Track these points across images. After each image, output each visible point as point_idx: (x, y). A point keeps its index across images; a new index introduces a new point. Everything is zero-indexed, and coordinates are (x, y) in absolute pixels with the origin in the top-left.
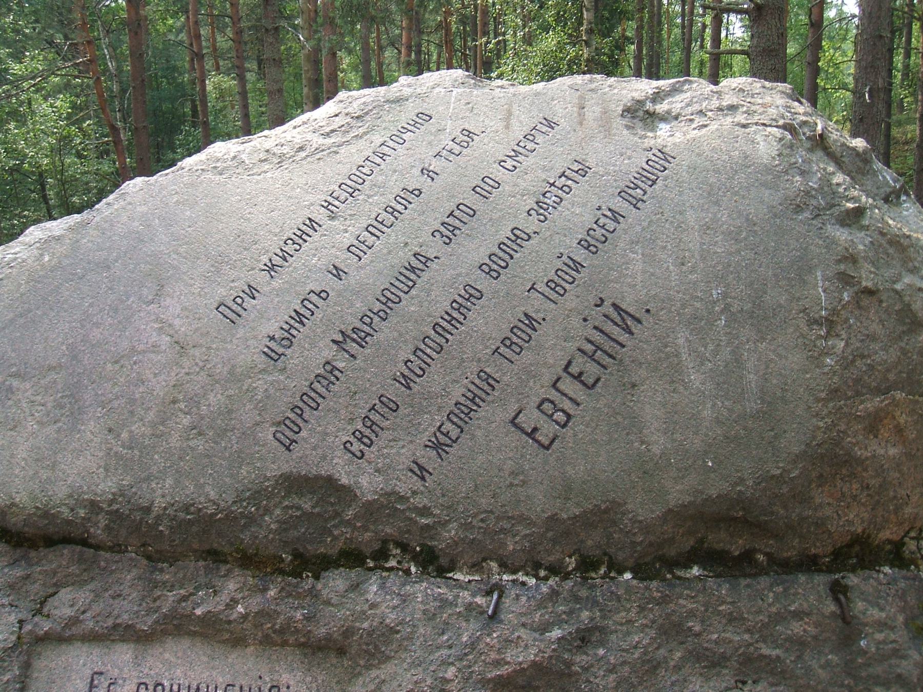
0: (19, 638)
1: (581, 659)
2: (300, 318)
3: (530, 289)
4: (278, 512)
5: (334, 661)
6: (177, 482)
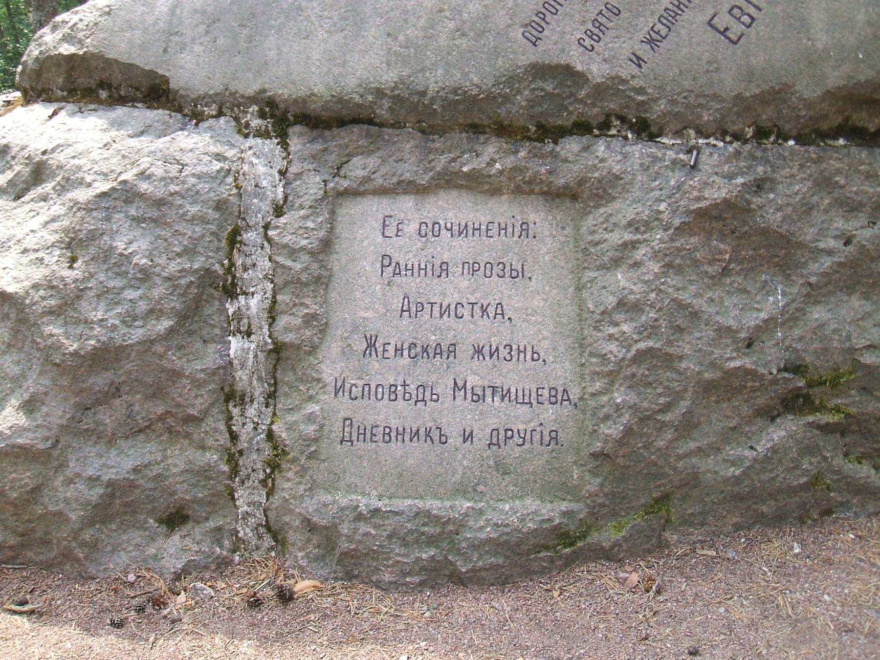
0: (325, 192)
1: (756, 201)
4: (527, 92)
5: (569, 205)
6: (447, 71)
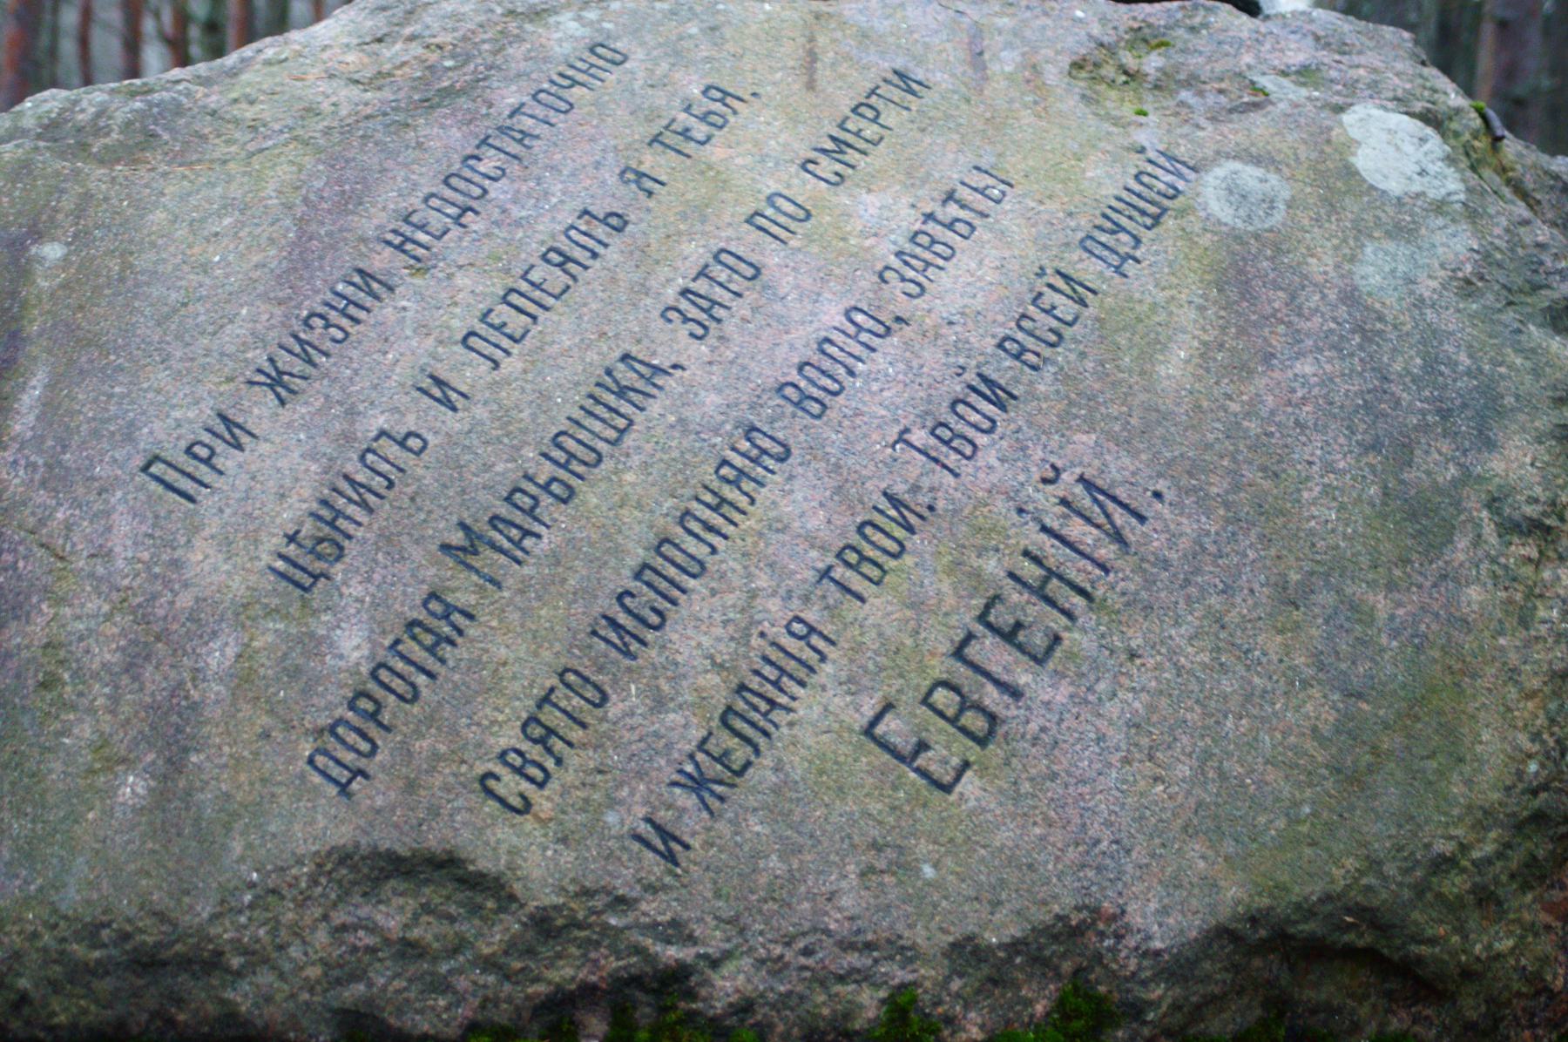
2: (360, 494)
3: (896, 442)
